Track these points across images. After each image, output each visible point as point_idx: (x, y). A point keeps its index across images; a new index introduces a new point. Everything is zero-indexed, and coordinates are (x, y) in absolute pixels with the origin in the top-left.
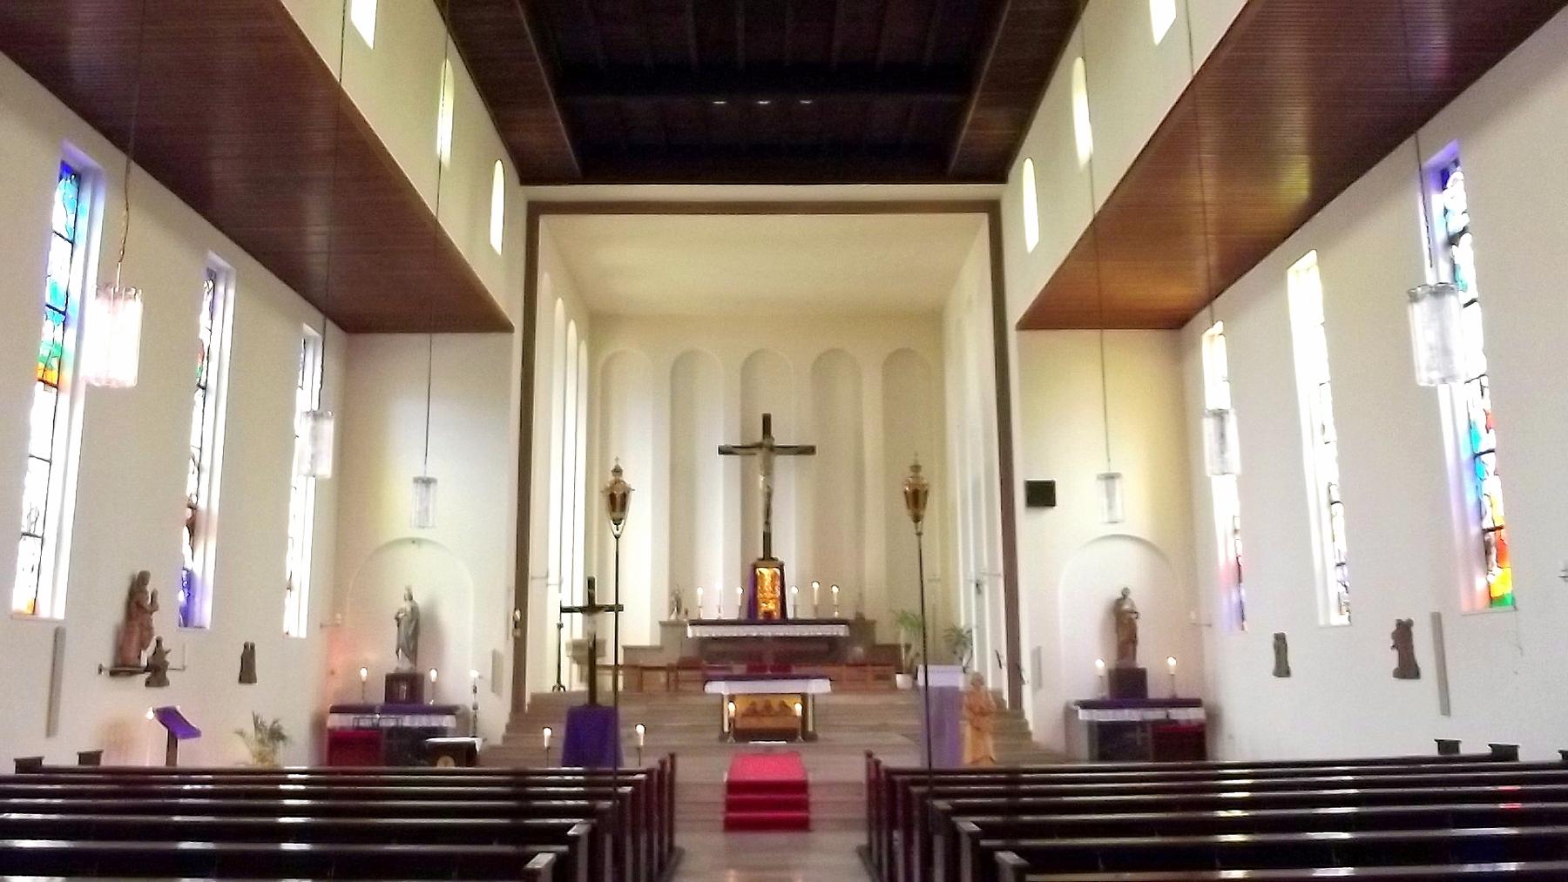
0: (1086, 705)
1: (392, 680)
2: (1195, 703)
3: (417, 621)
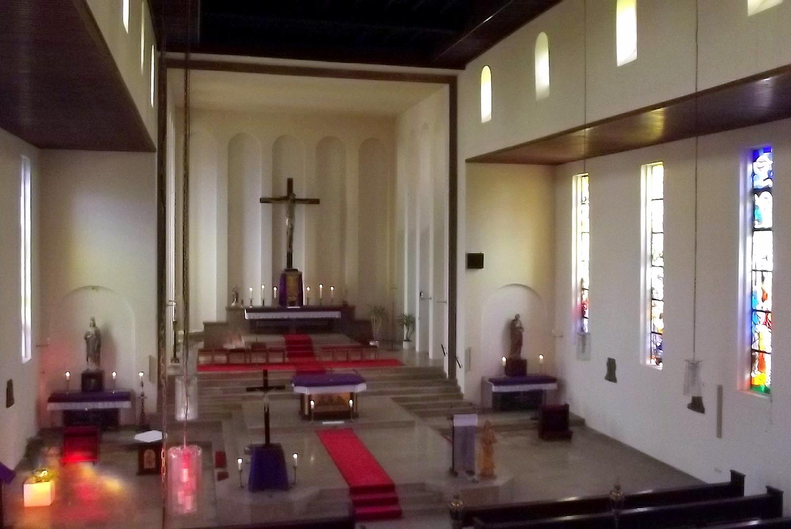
0: (497, 382)
1: (86, 377)
2: (552, 380)
3: (100, 341)
